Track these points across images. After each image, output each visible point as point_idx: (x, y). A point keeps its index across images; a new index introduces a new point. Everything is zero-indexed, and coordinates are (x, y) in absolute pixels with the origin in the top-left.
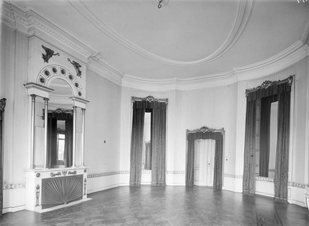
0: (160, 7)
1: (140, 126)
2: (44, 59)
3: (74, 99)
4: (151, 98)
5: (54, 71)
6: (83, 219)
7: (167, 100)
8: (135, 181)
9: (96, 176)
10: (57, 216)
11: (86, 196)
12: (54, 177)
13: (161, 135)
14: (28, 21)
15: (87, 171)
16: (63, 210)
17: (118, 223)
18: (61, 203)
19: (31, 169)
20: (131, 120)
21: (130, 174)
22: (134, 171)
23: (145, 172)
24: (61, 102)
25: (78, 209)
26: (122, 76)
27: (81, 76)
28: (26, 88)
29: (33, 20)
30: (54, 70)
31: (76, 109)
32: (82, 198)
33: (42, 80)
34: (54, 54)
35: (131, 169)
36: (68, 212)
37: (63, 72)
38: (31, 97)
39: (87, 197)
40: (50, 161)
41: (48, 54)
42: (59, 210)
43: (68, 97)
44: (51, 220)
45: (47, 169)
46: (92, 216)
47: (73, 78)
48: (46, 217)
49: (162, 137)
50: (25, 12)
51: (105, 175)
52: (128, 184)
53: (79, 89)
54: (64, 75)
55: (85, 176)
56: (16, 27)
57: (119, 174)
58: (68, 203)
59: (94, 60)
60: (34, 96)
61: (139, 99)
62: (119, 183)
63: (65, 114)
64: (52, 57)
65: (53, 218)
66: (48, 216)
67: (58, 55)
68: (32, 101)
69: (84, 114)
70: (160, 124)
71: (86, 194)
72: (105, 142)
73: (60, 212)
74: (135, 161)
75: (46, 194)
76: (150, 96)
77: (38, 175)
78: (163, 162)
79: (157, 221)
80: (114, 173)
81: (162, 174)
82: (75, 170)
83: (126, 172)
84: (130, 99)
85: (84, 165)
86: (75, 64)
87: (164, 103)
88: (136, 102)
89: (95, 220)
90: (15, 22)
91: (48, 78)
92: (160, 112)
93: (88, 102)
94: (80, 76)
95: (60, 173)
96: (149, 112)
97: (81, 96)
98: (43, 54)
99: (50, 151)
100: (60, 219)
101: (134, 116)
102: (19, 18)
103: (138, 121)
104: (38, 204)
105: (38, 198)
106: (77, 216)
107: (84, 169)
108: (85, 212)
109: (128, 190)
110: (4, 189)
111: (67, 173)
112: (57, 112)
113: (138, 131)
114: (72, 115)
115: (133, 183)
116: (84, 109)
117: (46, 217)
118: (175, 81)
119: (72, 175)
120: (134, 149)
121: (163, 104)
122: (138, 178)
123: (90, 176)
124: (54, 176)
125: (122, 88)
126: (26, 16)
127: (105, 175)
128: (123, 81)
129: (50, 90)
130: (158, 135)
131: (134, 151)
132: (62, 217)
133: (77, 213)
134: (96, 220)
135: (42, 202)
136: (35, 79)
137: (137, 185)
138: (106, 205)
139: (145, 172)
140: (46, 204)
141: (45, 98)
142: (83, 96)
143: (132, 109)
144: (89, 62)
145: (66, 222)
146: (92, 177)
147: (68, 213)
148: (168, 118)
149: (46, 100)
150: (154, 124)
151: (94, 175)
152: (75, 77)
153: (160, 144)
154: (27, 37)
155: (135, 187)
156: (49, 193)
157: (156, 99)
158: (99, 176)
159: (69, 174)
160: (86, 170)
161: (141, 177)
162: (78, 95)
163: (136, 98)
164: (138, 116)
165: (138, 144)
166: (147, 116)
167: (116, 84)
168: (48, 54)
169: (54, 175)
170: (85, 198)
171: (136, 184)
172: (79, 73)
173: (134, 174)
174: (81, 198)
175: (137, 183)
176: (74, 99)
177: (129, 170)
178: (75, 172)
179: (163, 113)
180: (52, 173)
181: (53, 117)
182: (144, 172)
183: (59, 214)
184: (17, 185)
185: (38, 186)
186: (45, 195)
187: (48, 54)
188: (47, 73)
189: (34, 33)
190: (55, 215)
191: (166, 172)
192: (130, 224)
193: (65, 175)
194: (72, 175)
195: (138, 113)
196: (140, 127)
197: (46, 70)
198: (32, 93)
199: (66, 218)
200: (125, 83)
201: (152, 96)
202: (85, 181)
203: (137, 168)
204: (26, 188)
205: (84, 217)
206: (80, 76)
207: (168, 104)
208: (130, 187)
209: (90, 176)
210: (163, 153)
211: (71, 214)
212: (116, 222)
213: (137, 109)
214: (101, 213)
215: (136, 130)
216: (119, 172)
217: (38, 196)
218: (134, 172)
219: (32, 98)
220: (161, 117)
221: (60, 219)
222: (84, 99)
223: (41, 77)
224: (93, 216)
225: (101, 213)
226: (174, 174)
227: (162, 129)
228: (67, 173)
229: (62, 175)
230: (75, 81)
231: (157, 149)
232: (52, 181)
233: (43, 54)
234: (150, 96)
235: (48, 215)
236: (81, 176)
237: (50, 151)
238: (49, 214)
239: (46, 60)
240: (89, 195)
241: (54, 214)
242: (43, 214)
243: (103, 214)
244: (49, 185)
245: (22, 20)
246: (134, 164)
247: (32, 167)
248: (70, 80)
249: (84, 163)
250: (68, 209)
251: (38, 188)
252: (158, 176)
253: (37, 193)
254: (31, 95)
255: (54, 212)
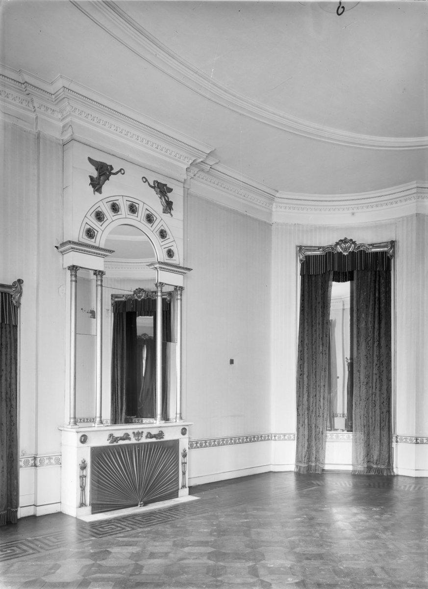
0: (342, 13)
1: (321, 319)
2: (94, 186)
3: (157, 266)
4: (348, 245)
5: (113, 209)
6: (168, 543)
7: (393, 244)
8: (309, 460)
9: (213, 443)
10: (118, 532)
11: (187, 490)
12: (115, 444)
13: (376, 341)
14: (61, 111)
15: (187, 432)
16: (133, 518)
17: (244, 561)
18: (132, 503)
19: (70, 427)
20: (297, 304)
21: (296, 441)
22: (306, 433)
23: (337, 437)
24: (133, 276)
25: (164, 520)
26: (272, 198)
27: (172, 211)
28: (60, 253)
29: (68, 108)
30: (115, 208)
31: (162, 289)
32: (178, 495)
33: (90, 233)
34: (113, 171)
35: (298, 429)
36: (141, 524)
37: (133, 209)
38: (69, 272)
39: (190, 494)
40: (124, 408)
41: (100, 175)
42: (123, 518)
43: (145, 264)
44: (104, 539)
45: (164, 422)
46: (187, 538)
47: (155, 219)
48: (96, 531)
49: (379, 344)
50: (53, 93)
51: (233, 441)
52: (292, 468)
53: (167, 243)
54: (136, 215)
55: (184, 444)
56: (39, 129)
57: (268, 440)
58: (145, 504)
59: (203, 170)
60: (74, 268)
61: (315, 250)
62: (269, 463)
63: (366, 254)
64: (109, 180)
65: (109, 535)
66: (101, 529)
67: (122, 172)
68: (71, 281)
69: (181, 300)
70: (375, 309)
71: (187, 486)
72: (232, 362)
73: (124, 522)
74: (308, 409)
75: (101, 482)
76: (346, 238)
77: (83, 438)
78: (385, 410)
79: (345, 566)
80: (256, 439)
81: (381, 444)
82: (160, 429)
83: (286, 437)
84: (293, 251)
85: (181, 418)
86: (158, 187)
87: (383, 253)
88: (308, 258)
89: (193, 548)
90: (37, 118)
91: (103, 228)
92: (373, 279)
93: (189, 270)
94: (170, 213)
95: (128, 435)
96: (345, 280)
97: (174, 258)
98: (90, 176)
99: (124, 385)
100: (120, 539)
101: (303, 296)
102: (43, 109)
103: (314, 307)
104: (84, 502)
105: (84, 489)
106: (158, 536)
107: (182, 427)
108: (177, 527)
109: (291, 483)
110: (21, 467)
111: (144, 435)
112: (136, 298)
113: (316, 331)
114: (168, 302)
115: (303, 465)
116: (180, 287)
117: (96, 531)
118: (414, 191)
119: (154, 440)
120: (305, 379)
121: (380, 256)
122: (317, 452)
123: (198, 445)
124: (115, 441)
125: (274, 227)
126: (57, 102)
127: (233, 441)
128: (274, 210)
129: (105, 252)
130: (369, 338)
131: (306, 383)
132: (126, 534)
133: (160, 528)
134: (197, 548)
135: (92, 498)
136: (76, 233)
137: (316, 471)
138: (227, 516)
139: (337, 437)
140: (100, 504)
141: (96, 271)
142: (178, 259)
143: (299, 277)
144: (192, 178)
145: (131, 548)
146: (201, 446)
147: (141, 526)
148: (398, 292)
149: (99, 274)
150: (358, 310)
151: (206, 442)
152: (158, 217)
153: (375, 362)
154: (59, 144)
155: (310, 476)
156: (105, 480)
157: (362, 245)
158: (219, 445)
159: (147, 437)
160: (184, 429)
161: (323, 449)
162: (167, 256)
163: (310, 248)
164: (314, 294)
165: (314, 365)
166: (340, 292)
167: (256, 220)
168: (101, 174)
169: (116, 440)
170: (184, 497)
171: (313, 468)
172: (168, 206)
173: (306, 441)
174: (175, 495)
175: (316, 466)
176: (157, 266)
177: (294, 431)
178: (161, 435)
179: (382, 281)
180: (111, 435)
181: (129, 309)
182: (334, 437)
183: (123, 526)
184: (45, 458)
185: (84, 462)
186: (98, 482)
187: (103, 173)
188: (99, 216)
189: (72, 135)
190: (113, 529)
191: (394, 439)
192: (272, 566)
193: (139, 440)
194: (154, 440)
195: (314, 285)
196: (321, 322)
197: (97, 210)
198: (71, 264)
199: (135, 537)
200: (280, 215)
201: (349, 238)
202: (185, 456)
203: (314, 426)
204: (62, 465)
205: (173, 538)
206: (170, 213)
207: (396, 256)
208: (298, 475)
209: (198, 445)
210: (385, 387)
211: (146, 529)
212: (239, 558)
213: (310, 276)
214: (211, 534)
215: (310, 330)
216: (268, 436)
217: (84, 484)
218: (306, 438)
219: (71, 272)
220: (375, 290)
221: (120, 539)
222: (181, 265)
223: (89, 227)
224: (191, 538)
225: (211, 534)
226: (418, 443)
227: (380, 323)
228: (144, 435)
229: (133, 441)
230: (159, 226)
231: (367, 377)
232: (111, 453)
233: (90, 176)
234: (346, 238)
235: (100, 527)
236: (175, 444)
237: (124, 385)
238: (102, 526)
239: (96, 188)
240: (193, 490)
241: (113, 526)
242: (93, 525)
243: (214, 536)
244: (106, 461)
245: (49, 112)
246: (306, 417)
247: (72, 420)
248: (149, 225)
249: (181, 414)
250: (143, 518)
251: (83, 467)
252: (372, 448)
253: (83, 477)
254: (69, 268)
255: (114, 522)
